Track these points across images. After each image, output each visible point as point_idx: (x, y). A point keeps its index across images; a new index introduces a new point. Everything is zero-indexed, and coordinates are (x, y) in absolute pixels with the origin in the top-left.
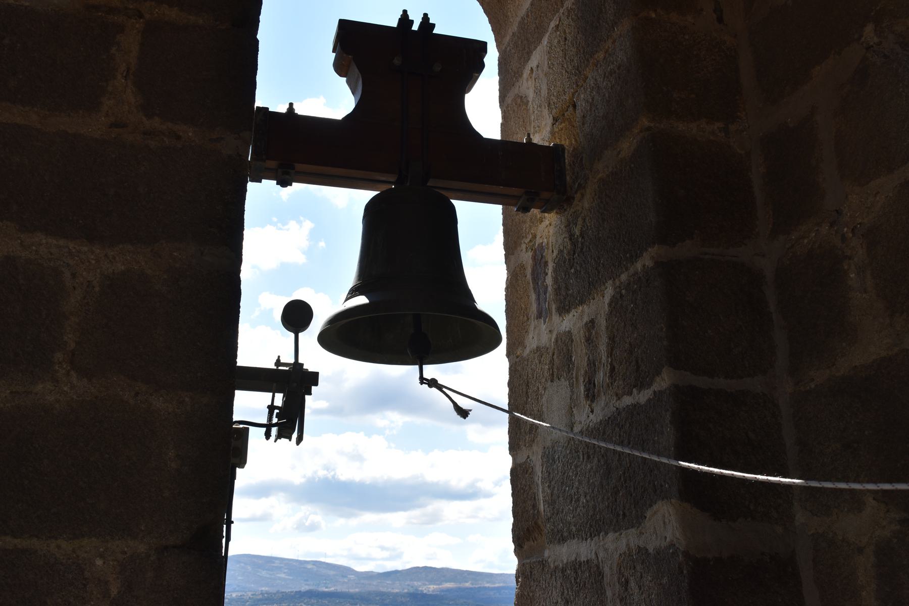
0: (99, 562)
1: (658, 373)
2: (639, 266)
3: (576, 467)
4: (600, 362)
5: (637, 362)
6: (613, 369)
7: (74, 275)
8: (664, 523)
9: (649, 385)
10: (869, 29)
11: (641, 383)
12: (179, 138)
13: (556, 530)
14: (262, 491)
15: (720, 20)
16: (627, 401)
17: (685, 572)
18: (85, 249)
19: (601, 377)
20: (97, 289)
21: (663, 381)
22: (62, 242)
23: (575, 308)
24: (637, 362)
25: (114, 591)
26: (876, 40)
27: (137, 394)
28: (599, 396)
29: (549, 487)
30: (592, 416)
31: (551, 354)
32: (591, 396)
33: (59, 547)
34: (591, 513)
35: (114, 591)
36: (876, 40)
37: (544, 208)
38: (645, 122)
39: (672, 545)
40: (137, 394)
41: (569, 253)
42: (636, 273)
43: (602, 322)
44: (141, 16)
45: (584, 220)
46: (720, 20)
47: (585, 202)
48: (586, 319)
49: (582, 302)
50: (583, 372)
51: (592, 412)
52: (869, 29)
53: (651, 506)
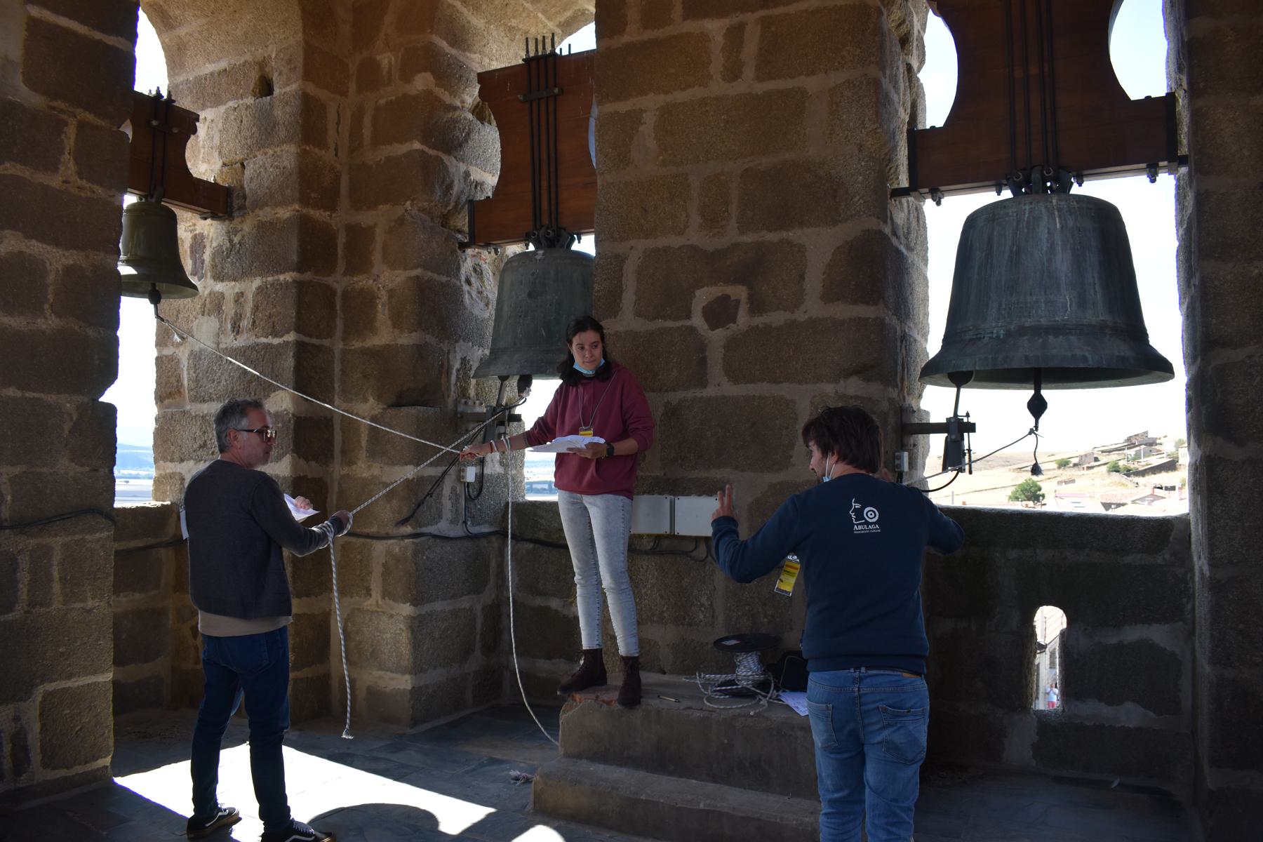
0: (68, 405)
1: (288, 333)
2: (282, 277)
3: (220, 365)
4: (246, 316)
5: (273, 323)
6: (254, 322)
7: (50, 264)
8: (282, 400)
9: (281, 336)
10: (408, 203)
11: (276, 334)
12: (94, 192)
13: (198, 396)
14: (953, 503)
15: (336, 155)
16: (263, 340)
17: (292, 422)
18: (54, 250)
19: (245, 323)
20: (61, 272)
21: (291, 337)
22: (44, 246)
23: (230, 281)
24: (273, 323)
25: (75, 418)
26: (410, 208)
27: (81, 327)
28: (242, 333)
29: (194, 372)
30: (235, 342)
31: (203, 300)
32: (236, 329)
33: (51, 398)
34: (230, 390)
35: (75, 418)
36: (410, 208)
37: (340, 323)
38: (297, 207)
39: (286, 410)
40: (81, 327)
41: (227, 249)
42: (278, 280)
43: (250, 296)
44: (75, 117)
45: (243, 236)
46: (336, 155)
47: (247, 226)
48: (237, 290)
49: (235, 280)
50: (230, 317)
51: (236, 339)
52: (408, 203)
53: (274, 391)
